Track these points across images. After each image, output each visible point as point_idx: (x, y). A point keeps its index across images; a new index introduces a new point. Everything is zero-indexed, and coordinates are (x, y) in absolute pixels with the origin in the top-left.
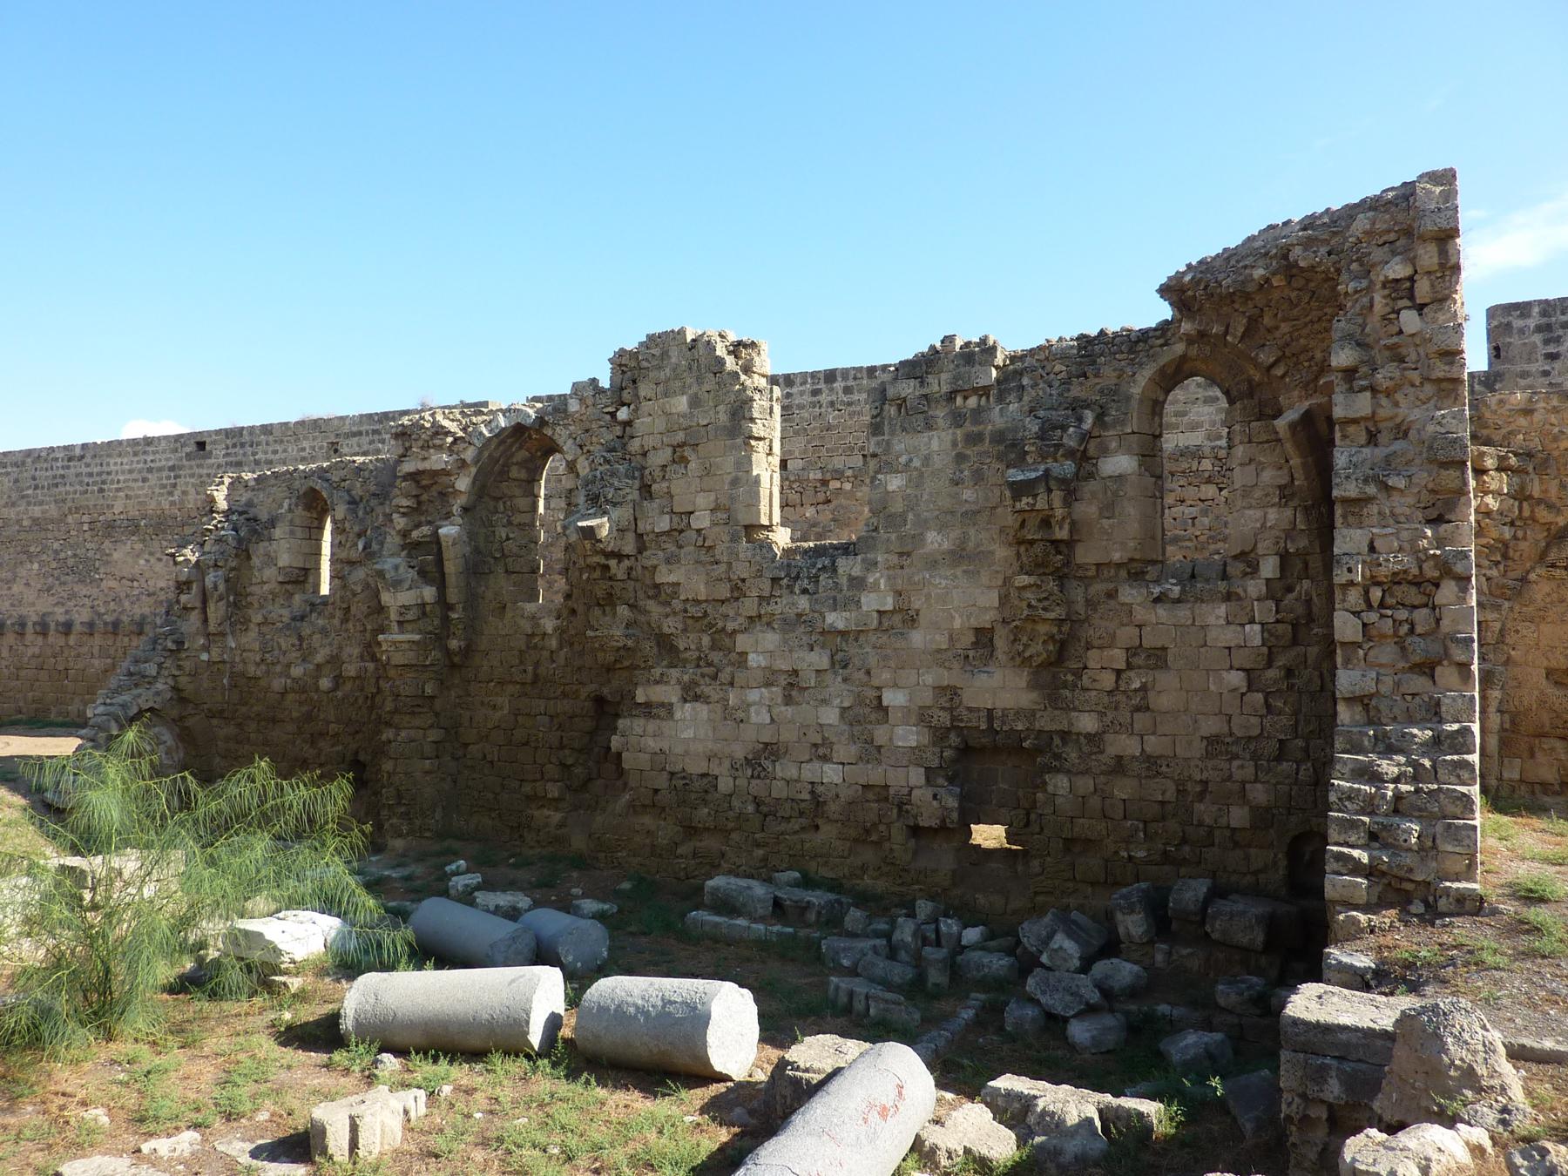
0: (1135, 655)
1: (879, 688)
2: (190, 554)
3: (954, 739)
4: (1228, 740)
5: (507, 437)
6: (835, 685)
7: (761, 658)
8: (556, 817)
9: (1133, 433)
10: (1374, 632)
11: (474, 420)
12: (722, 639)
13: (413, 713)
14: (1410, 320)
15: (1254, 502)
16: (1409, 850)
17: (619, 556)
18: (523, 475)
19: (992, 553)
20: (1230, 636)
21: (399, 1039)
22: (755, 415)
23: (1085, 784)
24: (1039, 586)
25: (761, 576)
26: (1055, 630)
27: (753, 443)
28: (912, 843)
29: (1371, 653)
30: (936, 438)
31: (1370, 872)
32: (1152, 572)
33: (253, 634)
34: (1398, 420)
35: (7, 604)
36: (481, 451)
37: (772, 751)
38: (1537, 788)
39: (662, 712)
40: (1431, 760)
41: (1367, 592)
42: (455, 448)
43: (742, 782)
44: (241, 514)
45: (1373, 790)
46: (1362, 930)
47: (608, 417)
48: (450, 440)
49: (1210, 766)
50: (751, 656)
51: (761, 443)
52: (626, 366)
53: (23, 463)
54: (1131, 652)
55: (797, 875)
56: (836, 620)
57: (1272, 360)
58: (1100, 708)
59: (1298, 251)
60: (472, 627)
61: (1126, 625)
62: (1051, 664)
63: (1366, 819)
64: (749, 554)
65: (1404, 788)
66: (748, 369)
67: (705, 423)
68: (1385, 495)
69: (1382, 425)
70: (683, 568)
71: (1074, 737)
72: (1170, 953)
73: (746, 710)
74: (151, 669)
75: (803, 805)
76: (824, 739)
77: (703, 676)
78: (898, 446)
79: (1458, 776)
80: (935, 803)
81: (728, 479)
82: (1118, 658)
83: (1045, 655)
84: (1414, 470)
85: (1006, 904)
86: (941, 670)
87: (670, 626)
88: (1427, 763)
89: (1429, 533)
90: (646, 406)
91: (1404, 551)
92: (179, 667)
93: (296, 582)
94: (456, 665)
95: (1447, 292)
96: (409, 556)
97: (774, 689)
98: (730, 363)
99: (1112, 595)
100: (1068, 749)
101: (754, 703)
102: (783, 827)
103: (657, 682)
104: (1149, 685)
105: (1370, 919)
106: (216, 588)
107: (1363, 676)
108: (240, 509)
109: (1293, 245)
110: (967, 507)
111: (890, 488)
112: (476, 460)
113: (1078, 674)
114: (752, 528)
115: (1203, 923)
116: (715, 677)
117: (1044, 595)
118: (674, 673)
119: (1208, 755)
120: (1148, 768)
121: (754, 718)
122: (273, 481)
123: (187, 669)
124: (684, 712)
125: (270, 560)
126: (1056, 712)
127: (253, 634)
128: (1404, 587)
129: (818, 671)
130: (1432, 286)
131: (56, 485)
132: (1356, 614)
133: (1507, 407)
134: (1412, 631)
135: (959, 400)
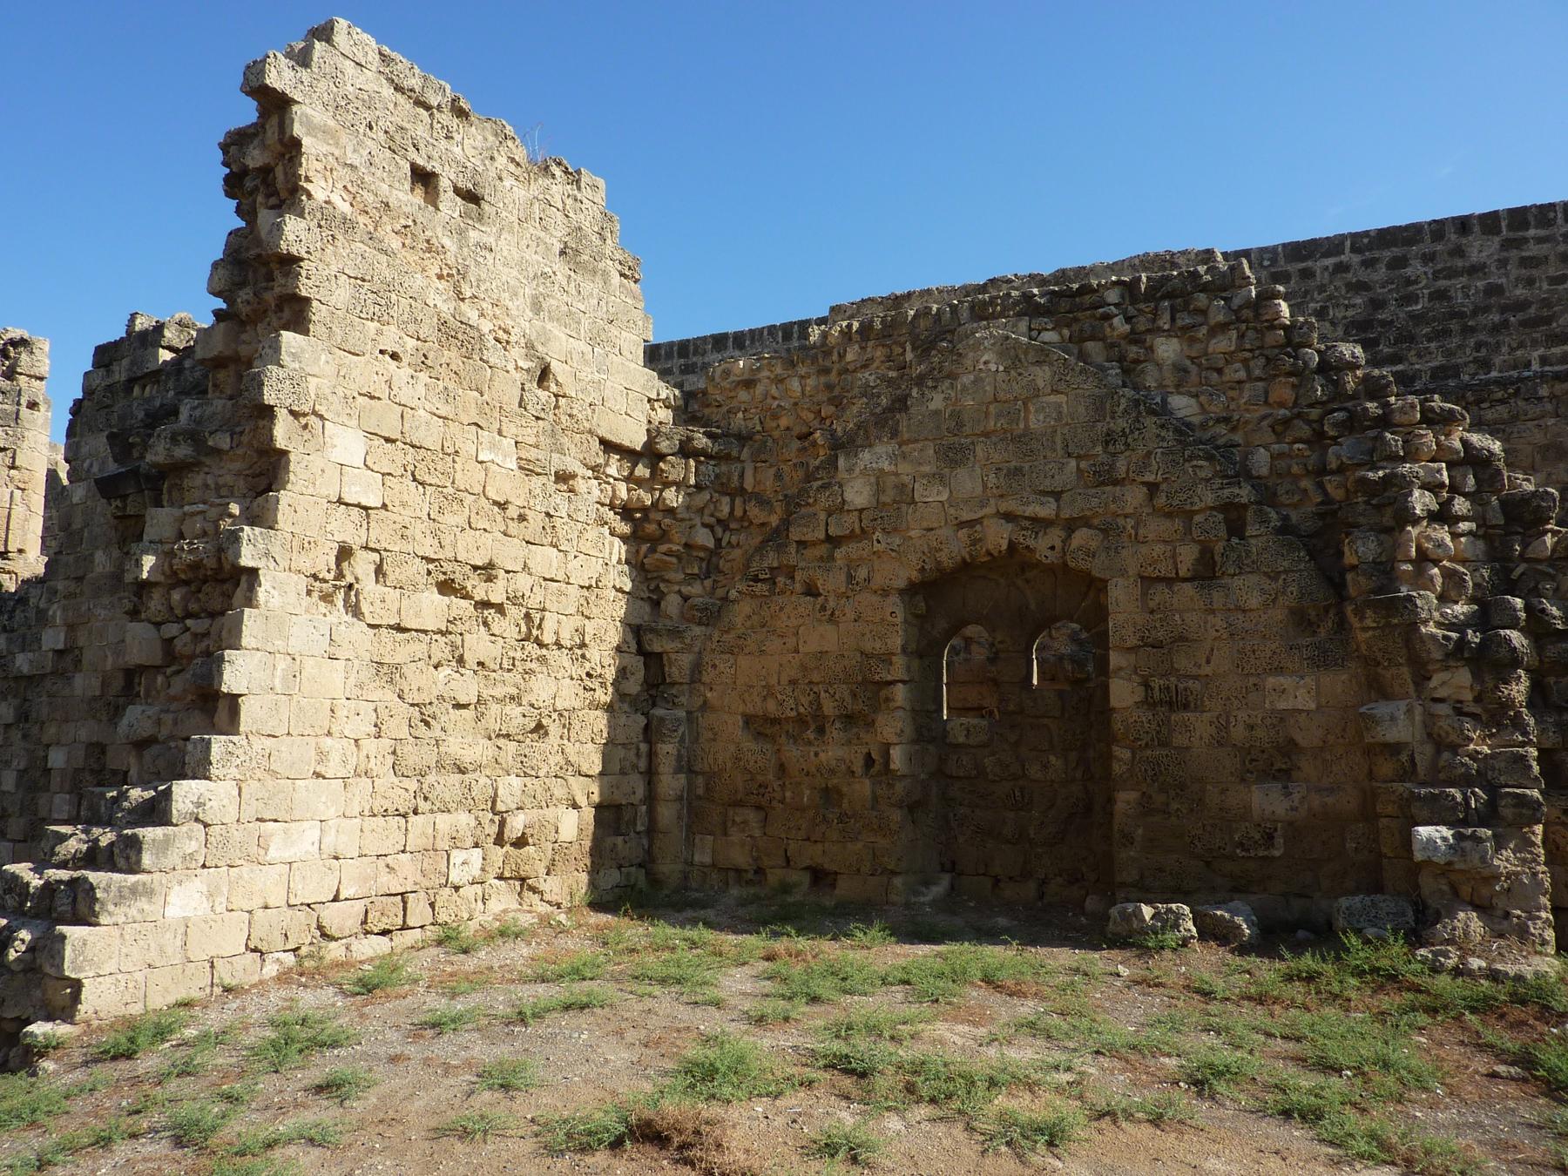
38: (732, 874)
132: (158, 625)
133: (732, 378)
135: (137, 391)
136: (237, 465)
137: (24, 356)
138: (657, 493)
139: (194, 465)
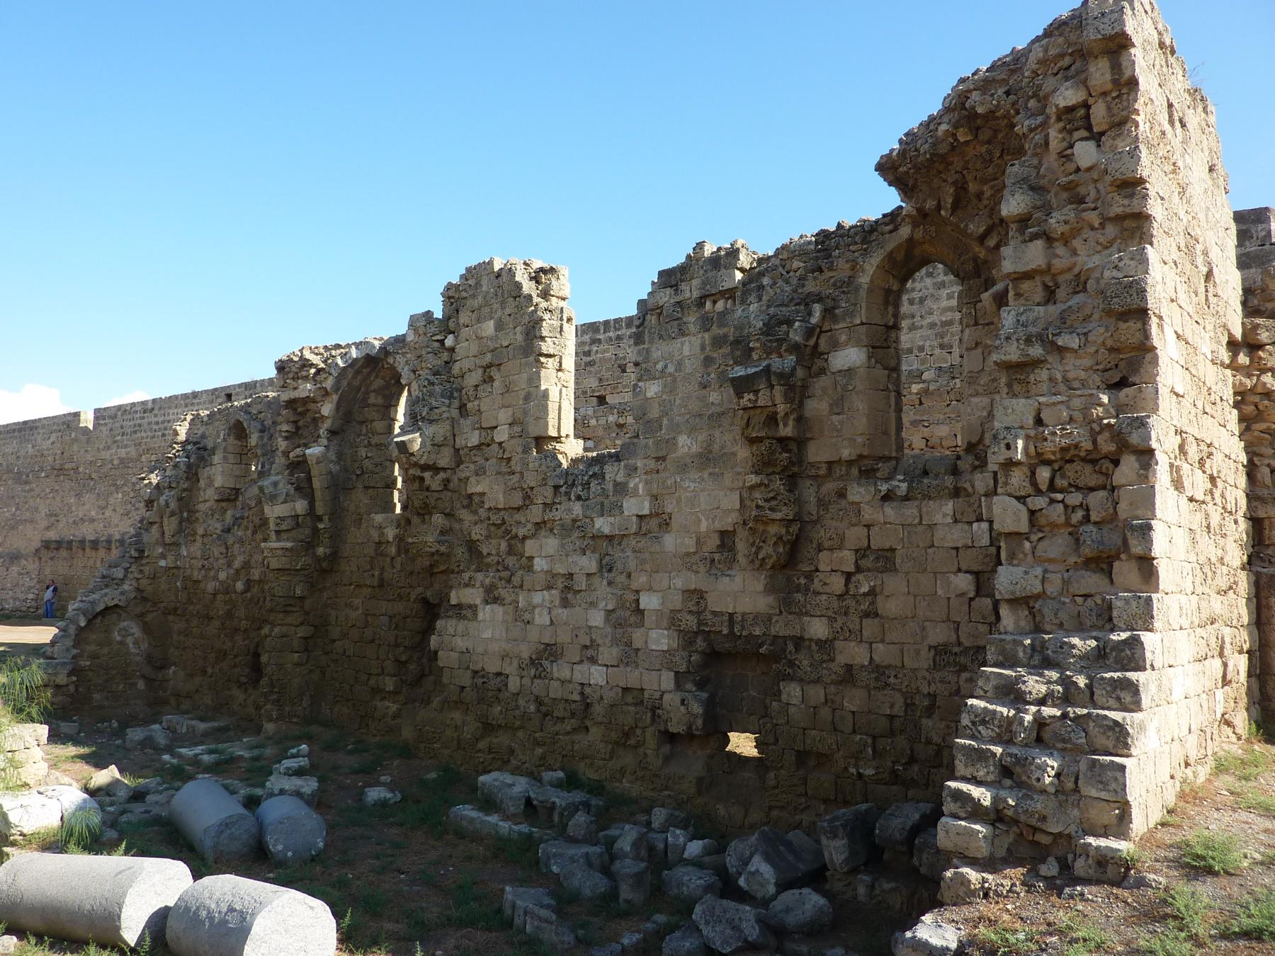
0: (864, 556)
1: (637, 592)
2: (154, 479)
3: (700, 643)
4: (956, 649)
5: (362, 366)
6: (601, 586)
7: (544, 562)
8: (394, 707)
9: (863, 324)
10: (1043, 521)
11: (333, 353)
12: (515, 543)
13: (286, 612)
14: (1085, 153)
15: (980, 389)
16: (1043, 791)
17: (435, 469)
18: (380, 401)
19: (734, 454)
20: (957, 536)
21: (26, 921)
22: (545, 333)
23: (817, 694)
24: (767, 486)
25: (546, 484)
26: (783, 531)
27: (543, 359)
28: (666, 748)
29: (1041, 546)
30: (687, 343)
31: (995, 816)
32: (884, 468)
33: (198, 544)
34: (1076, 270)
35: (101, 525)
36: (338, 380)
37: (551, 651)
39: (469, 613)
40: (1089, 677)
41: (1033, 473)
42: (318, 378)
43: (526, 681)
44: (195, 444)
45: (1012, 712)
46: (973, 893)
47: (437, 344)
48: (313, 371)
49: (937, 678)
50: (536, 561)
51: (551, 360)
52: (453, 297)
53: (116, 416)
54: (861, 553)
55: (560, 774)
56: (603, 525)
57: (982, 229)
58: (830, 613)
59: (975, 96)
60: (337, 537)
61: (855, 525)
62: (784, 567)
63: (998, 750)
64: (536, 464)
65: (1048, 711)
66: (545, 294)
67: (505, 344)
68: (1057, 358)
69: (1061, 279)
70: (487, 479)
71: (807, 643)
72: (872, 887)
73: (532, 612)
74: (119, 573)
75: (573, 706)
76: (592, 641)
77: (501, 579)
78: (656, 354)
79: (1118, 699)
80: (682, 708)
81: (523, 393)
82: (847, 559)
83: (774, 557)
84: (1091, 326)
85: (746, 816)
86: (689, 574)
87: (477, 532)
88: (1081, 681)
89: (1105, 399)
90: (465, 332)
91: (1075, 422)
92: (141, 571)
93: (228, 500)
94: (328, 568)
95: (1124, 113)
96: (291, 474)
97: (554, 592)
98: (528, 287)
99: (842, 494)
100: (799, 656)
101: (538, 606)
102: (558, 727)
103: (466, 585)
104: (878, 589)
105: (984, 881)
106: (167, 505)
107: (1026, 573)
108: (195, 440)
109: (970, 91)
110: (713, 409)
111: (649, 395)
112: (337, 387)
113: (809, 576)
114: (541, 440)
115: (911, 854)
116: (509, 581)
117: (771, 495)
118: (480, 576)
119: (935, 666)
120: (877, 679)
121: (538, 620)
122: (218, 416)
123: (147, 573)
124: (486, 612)
125: (210, 482)
126: (791, 617)
127: (198, 544)
128: (1077, 466)
129: (588, 575)
130: (1109, 108)
131: (135, 432)
132: (1021, 499)
134: (1087, 519)
135: (708, 305)
136: (1088, 362)
137: (554, 282)
138: (1255, 378)
139: (1042, 362)
